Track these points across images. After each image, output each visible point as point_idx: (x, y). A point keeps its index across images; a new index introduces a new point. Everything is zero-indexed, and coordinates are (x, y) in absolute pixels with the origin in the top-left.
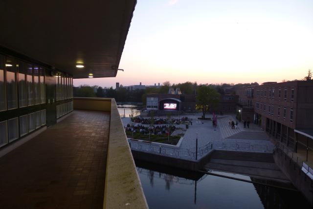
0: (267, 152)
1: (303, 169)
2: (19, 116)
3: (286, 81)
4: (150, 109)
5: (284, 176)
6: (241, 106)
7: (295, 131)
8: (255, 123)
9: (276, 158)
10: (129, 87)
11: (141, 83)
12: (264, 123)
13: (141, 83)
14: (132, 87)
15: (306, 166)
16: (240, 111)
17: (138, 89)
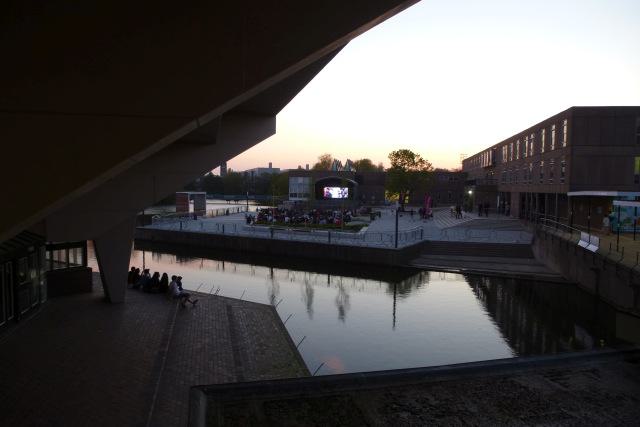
0: (522, 242)
1: (582, 243)
2: (52, 271)
3: (501, 335)
4: (297, 199)
5: (546, 265)
6: (471, 183)
7: (570, 194)
8: (499, 212)
9: (536, 251)
10: (246, 173)
11: (270, 164)
12: (515, 203)
13: (270, 164)
14: (253, 171)
15: (584, 235)
16: (470, 192)
17: (267, 174)
